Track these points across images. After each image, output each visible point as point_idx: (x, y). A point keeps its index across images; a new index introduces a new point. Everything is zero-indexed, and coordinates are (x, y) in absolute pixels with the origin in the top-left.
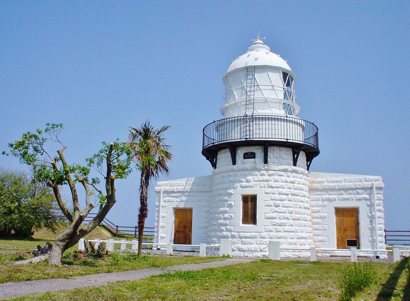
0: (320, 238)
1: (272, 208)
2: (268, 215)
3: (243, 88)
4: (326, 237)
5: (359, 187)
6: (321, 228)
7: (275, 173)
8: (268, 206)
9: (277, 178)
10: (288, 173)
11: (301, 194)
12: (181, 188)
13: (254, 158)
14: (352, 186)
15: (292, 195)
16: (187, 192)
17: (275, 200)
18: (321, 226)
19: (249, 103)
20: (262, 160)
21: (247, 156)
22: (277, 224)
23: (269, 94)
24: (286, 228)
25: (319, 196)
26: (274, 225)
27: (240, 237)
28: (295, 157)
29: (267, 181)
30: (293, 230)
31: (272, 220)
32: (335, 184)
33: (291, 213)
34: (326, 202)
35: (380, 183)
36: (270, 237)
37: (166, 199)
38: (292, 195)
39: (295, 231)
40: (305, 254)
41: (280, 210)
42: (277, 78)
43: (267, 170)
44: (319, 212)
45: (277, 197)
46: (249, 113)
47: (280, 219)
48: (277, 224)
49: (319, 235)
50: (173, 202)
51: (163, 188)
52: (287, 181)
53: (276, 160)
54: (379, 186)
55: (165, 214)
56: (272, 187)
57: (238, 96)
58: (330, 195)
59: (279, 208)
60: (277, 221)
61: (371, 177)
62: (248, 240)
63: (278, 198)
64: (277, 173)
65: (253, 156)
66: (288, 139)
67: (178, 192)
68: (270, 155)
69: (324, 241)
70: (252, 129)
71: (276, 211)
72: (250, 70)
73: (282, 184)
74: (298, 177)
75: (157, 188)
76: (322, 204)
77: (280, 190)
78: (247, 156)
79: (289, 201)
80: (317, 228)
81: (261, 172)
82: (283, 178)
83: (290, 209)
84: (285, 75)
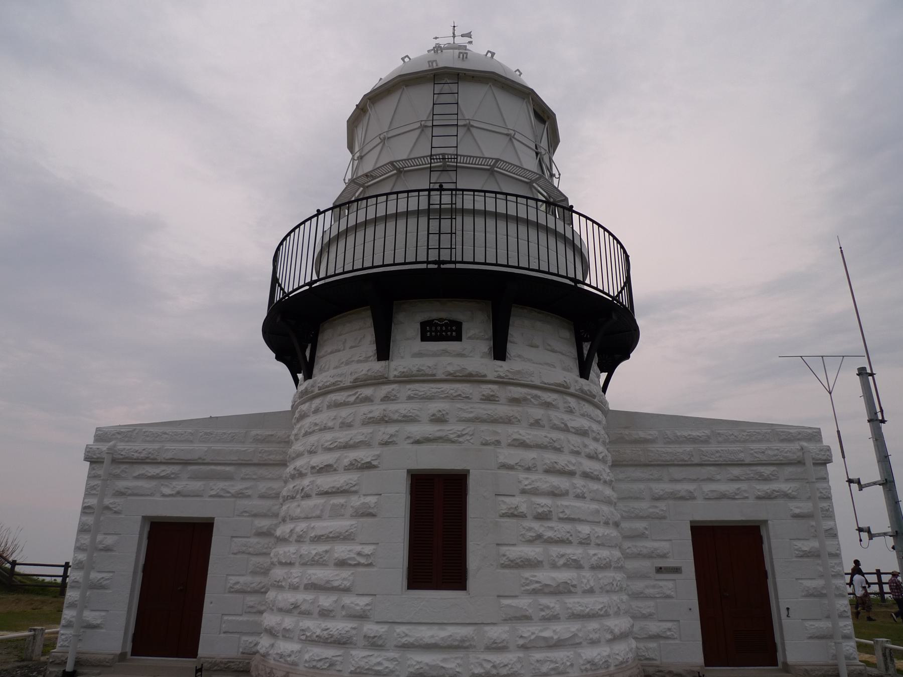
0: (654, 627)
1: (527, 524)
4: (669, 625)
5: (763, 457)
7: (529, 397)
8: (513, 515)
9: (537, 413)
13: (459, 338)
17: (535, 492)
18: (654, 587)
20: (485, 346)
21: (431, 331)
22: (546, 590)
24: (574, 602)
25: (642, 486)
26: (535, 592)
28: (586, 352)
31: (527, 574)
34: (662, 505)
36: (521, 642)
39: (602, 613)
41: (549, 534)
44: (641, 536)
47: (554, 566)
50: (142, 495)
52: (569, 425)
58: (673, 480)
60: (545, 576)
63: (544, 486)
64: (536, 397)
65: (452, 331)
68: (515, 334)
69: (667, 638)
71: (539, 537)
73: (555, 435)
76: (651, 510)
78: (435, 332)
82: (557, 416)
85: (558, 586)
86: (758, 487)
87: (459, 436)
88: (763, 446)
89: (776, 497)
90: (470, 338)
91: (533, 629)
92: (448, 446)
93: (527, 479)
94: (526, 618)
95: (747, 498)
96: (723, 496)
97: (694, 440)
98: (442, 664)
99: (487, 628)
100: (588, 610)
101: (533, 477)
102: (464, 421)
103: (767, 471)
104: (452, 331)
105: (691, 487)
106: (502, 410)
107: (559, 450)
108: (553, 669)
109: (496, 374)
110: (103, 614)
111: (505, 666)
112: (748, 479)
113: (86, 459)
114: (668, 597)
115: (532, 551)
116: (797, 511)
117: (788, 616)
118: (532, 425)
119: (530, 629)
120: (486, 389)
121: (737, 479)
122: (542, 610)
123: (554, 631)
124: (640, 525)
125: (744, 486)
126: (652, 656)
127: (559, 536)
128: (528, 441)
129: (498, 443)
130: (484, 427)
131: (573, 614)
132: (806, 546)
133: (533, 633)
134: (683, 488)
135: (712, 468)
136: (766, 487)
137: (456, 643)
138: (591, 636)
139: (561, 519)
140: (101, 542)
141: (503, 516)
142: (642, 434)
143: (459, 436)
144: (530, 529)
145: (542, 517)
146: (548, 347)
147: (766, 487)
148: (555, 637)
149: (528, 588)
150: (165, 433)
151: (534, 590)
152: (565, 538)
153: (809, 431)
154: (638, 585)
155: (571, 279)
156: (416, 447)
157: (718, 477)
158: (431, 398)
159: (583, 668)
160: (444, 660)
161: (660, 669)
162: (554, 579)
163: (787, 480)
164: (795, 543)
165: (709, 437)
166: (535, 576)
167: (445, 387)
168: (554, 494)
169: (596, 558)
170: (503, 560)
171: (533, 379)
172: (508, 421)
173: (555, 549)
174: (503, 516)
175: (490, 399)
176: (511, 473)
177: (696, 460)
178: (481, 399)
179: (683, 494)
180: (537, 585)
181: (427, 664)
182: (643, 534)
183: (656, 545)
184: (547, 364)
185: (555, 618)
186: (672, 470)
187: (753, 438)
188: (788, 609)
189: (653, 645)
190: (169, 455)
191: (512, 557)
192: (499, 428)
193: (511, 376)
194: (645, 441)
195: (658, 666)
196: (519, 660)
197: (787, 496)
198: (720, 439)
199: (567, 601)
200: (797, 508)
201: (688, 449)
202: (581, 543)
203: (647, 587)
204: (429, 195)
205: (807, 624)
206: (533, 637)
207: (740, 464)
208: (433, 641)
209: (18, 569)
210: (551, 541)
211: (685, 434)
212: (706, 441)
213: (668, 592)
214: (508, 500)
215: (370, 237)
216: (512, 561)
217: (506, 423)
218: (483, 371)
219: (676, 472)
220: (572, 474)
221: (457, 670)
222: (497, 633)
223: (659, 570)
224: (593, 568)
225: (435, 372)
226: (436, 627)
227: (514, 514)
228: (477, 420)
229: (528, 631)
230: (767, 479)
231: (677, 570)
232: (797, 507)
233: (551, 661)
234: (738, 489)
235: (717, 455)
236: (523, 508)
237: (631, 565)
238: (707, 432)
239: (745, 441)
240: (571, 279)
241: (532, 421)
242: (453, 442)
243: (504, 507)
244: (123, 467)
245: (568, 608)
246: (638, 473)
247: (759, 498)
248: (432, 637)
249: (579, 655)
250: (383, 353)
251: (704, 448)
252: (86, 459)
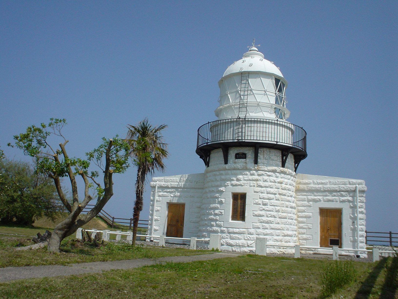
0: (305, 236)
1: (261, 206)
2: (256, 213)
3: (237, 92)
9: (266, 178)
12: (175, 184)
13: (245, 158)
14: (336, 189)
15: (280, 194)
16: (181, 188)
17: (264, 198)
19: (243, 106)
20: (252, 160)
23: (261, 99)
26: (261, 222)
27: (229, 233)
29: (257, 180)
30: (280, 227)
31: (260, 218)
32: (320, 186)
33: (278, 211)
34: (311, 203)
35: (363, 187)
37: (161, 194)
38: (280, 194)
41: (267, 209)
42: (269, 84)
43: (257, 170)
45: (265, 195)
46: (242, 116)
47: (267, 217)
49: (304, 234)
51: (158, 183)
53: (266, 162)
54: (362, 189)
55: (159, 208)
56: (261, 187)
57: (231, 99)
58: (315, 196)
60: (264, 219)
61: (354, 181)
62: (237, 235)
63: (266, 197)
64: (266, 174)
67: (172, 188)
68: (260, 156)
70: (244, 131)
71: (264, 209)
72: (244, 75)
73: (270, 184)
75: (152, 183)
77: (269, 189)
81: (252, 172)
82: (272, 179)
83: (278, 208)
84: (277, 80)
136: (342, 198)
139: (270, 205)
147: (342, 198)
168: (269, 199)
202: (276, 212)
209: (115, 220)
215: (222, 127)
250: (226, 162)
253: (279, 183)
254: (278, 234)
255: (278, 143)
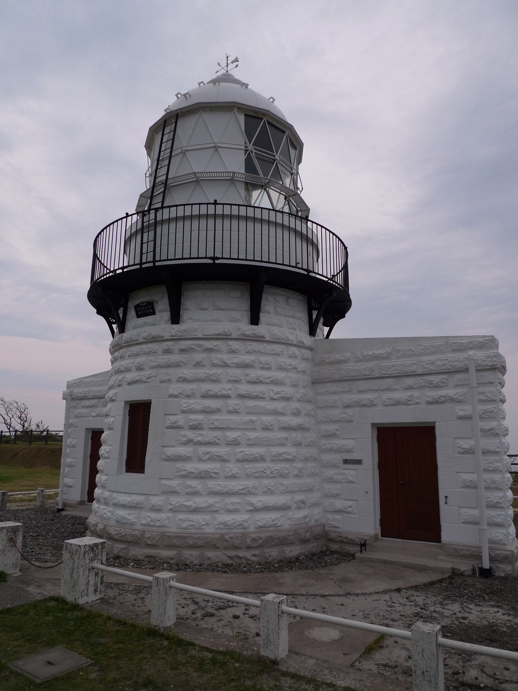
0: (339, 504)
1: (183, 432)
2: (170, 451)
4: (351, 503)
5: (432, 368)
6: (340, 477)
7: (194, 347)
8: (173, 428)
10: (231, 343)
11: (272, 395)
13: (154, 313)
14: (414, 368)
15: (242, 397)
17: (191, 411)
18: (342, 474)
20: (167, 315)
22: (191, 476)
24: (212, 484)
25: (336, 397)
28: (314, 317)
30: (237, 488)
31: (179, 465)
32: (371, 364)
33: (235, 443)
34: (350, 411)
36: (170, 507)
38: (242, 397)
40: (273, 553)
41: (200, 439)
44: (333, 436)
47: (200, 460)
48: (191, 476)
49: (336, 496)
58: (360, 392)
59: (201, 432)
60: (190, 467)
63: (198, 407)
64: (199, 346)
66: (218, 258)
69: (348, 513)
74: (263, 351)
76: (342, 415)
77: (206, 387)
79: (229, 412)
80: (332, 478)
82: (215, 357)
83: (232, 435)
85: (200, 473)
86: (428, 393)
87: (148, 378)
88: (433, 358)
89: (443, 402)
90: (159, 312)
91: (178, 500)
92: (143, 385)
93: (187, 403)
94: (174, 493)
95: (418, 403)
96: (397, 403)
97: (377, 358)
98: (128, 517)
99: (151, 497)
100: (226, 490)
101: (191, 401)
102: (152, 368)
103: (436, 379)
104: (150, 309)
105: (371, 396)
106: (175, 358)
107: (216, 381)
108: (191, 526)
109: (170, 334)
110: (73, 480)
111: (159, 520)
112: (420, 387)
113: (64, 399)
114: (351, 482)
115: (181, 450)
116: (461, 413)
117: (446, 503)
118: (194, 366)
119: (176, 499)
120: (165, 345)
121: (410, 388)
122: (187, 488)
123: (194, 502)
124: (332, 427)
125: (416, 393)
126: (337, 525)
127: (207, 440)
128: (188, 378)
129: (169, 381)
130: (162, 371)
131: (212, 492)
132: (466, 444)
133: (178, 502)
134: (365, 397)
135: (390, 380)
136: (434, 394)
137: (134, 505)
138: (228, 507)
140: (71, 443)
141: (168, 428)
142: (338, 357)
143: (148, 378)
144: (185, 436)
145: (194, 428)
146: (216, 308)
147: (434, 394)
148: (194, 506)
149: (178, 474)
150: (92, 382)
151: (182, 475)
152: (212, 441)
153: (481, 340)
154: (330, 473)
155: (211, 258)
156: (129, 387)
157: (396, 387)
158: (137, 355)
159: (217, 527)
160: (129, 514)
161: (341, 535)
162: (197, 468)
163: (456, 386)
164: (458, 441)
165: (389, 354)
166: (184, 466)
167: (144, 346)
169: (242, 454)
170: (164, 456)
171: (196, 333)
172: (177, 365)
173: (202, 448)
174: (168, 428)
175: (167, 351)
176: (176, 399)
177: (377, 374)
178: (163, 353)
179: (365, 402)
180: (184, 472)
181: (120, 516)
182: (335, 434)
183: (344, 442)
184: (214, 320)
185: (196, 493)
186: (359, 383)
187: (428, 351)
188: (446, 497)
189: (338, 517)
190: (92, 394)
191: (168, 454)
192: (171, 371)
193: (179, 334)
194: (340, 362)
195: (339, 533)
196: (168, 518)
197: (452, 400)
198: (399, 355)
199: (208, 483)
200: (462, 410)
201: (370, 366)
203: (336, 474)
204: (213, 204)
205: (463, 511)
206: (178, 505)
207: (414, 375)
208: (123, 503)
210: (200, 443)
211: (371, 353)
212: (388, 357)
213: (351, 479)
214: (171, 418)
216: (169, 457)
217: (176, 367)
218: (162, 333)
219: (362, 385)
220: (227, 397)
221: (134, 520)
222: (156, 500)
223: (346, 462)
224: (238, 461)
225: (137, 338)
226: (128, 495)
227: (175, 427)
228: (159, 366)
229: (175, 500)
230: (437, 387)
231: (359, 462)
232: (461, 410)
233: (190, 520)
234: (411, 396)
235: (394, 368)
236: (181, 423)
237: (326, 457)
238: (389, 350)
239: (420, 355)
240: (211, 258)
241: (194, 363)
242: (145, 382)
243: (168, 422)
244: (77, 401)
245: (208, 488)
246: (334, 387)
247: (429, 403)
248: (124, 500)
249: (216, 518)
251: (385, 363)
252: (64, 399)
253: (239, 366)
254: (231, 507)
255: (217, 262)
